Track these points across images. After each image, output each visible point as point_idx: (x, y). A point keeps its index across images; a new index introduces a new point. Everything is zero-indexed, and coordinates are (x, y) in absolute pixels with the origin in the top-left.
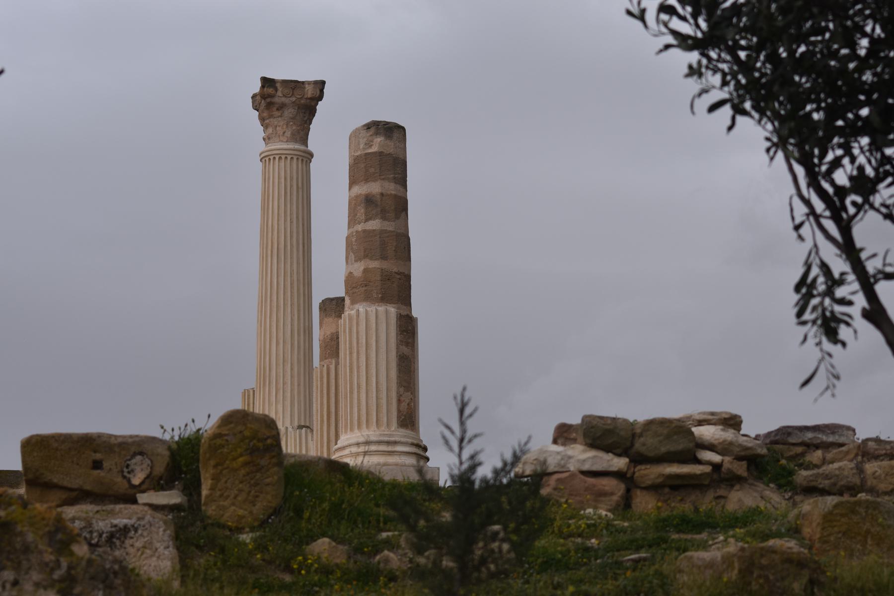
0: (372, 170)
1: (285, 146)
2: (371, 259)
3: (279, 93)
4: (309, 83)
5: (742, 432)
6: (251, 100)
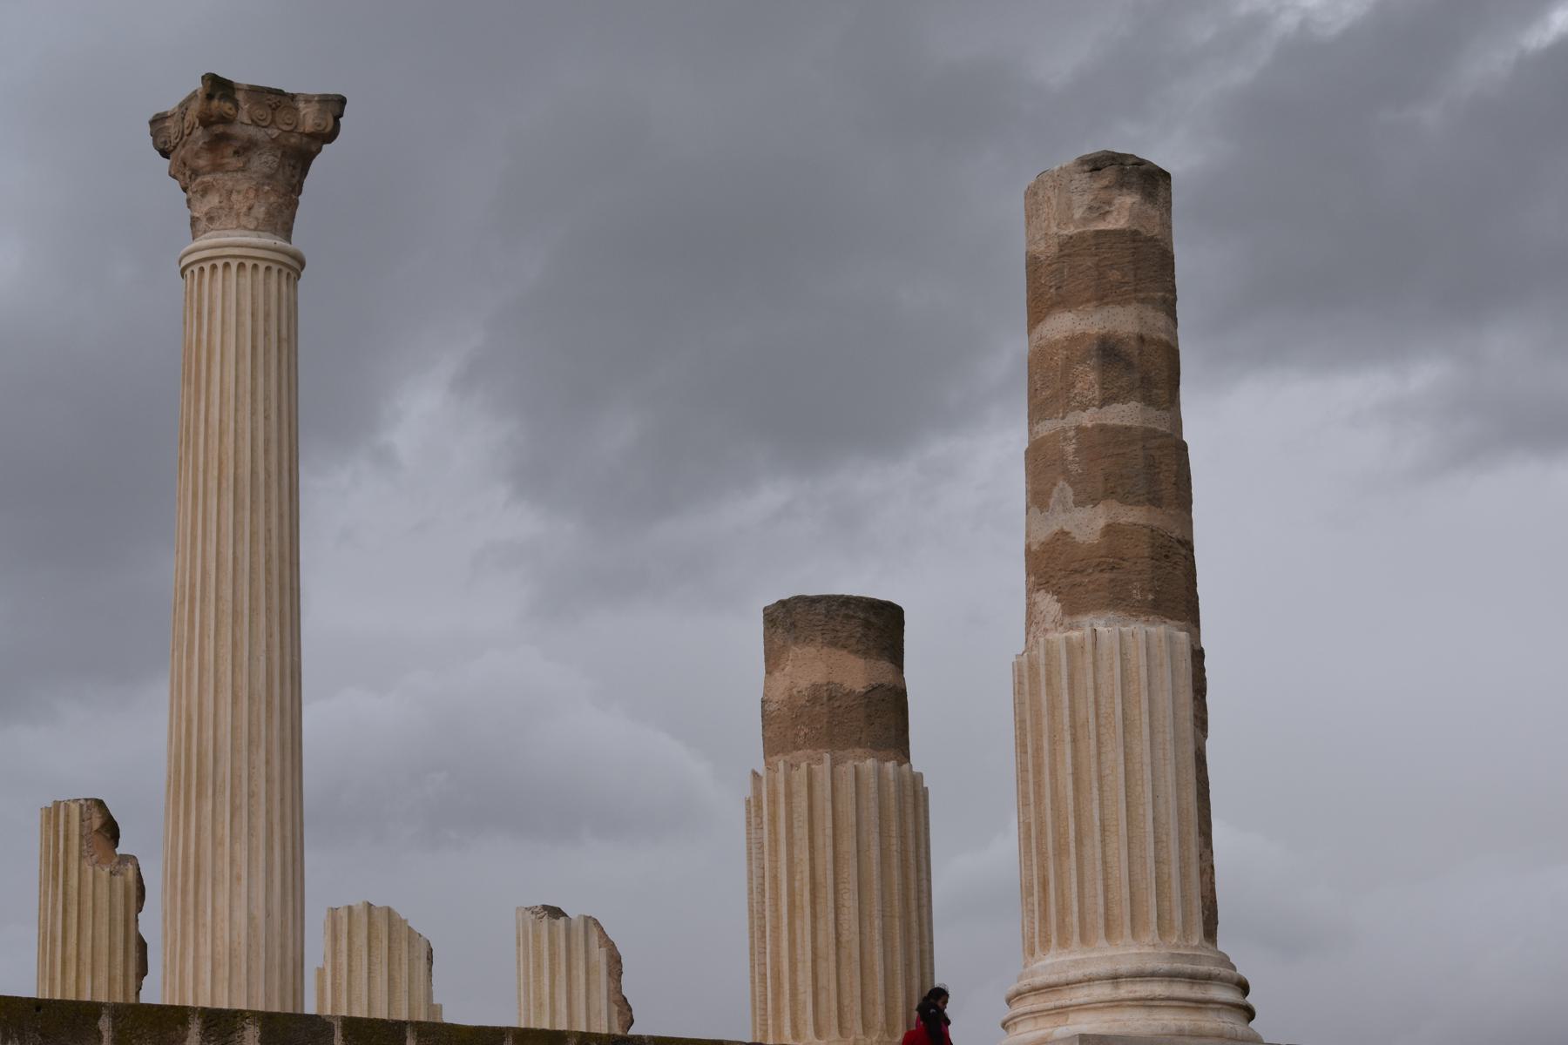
0: (1115, 275)
1: (253, 239)
2: (1123, 501)
3: (243, 116)
4: (308, 99)
5: (119, 851)
6: (148, 129)
